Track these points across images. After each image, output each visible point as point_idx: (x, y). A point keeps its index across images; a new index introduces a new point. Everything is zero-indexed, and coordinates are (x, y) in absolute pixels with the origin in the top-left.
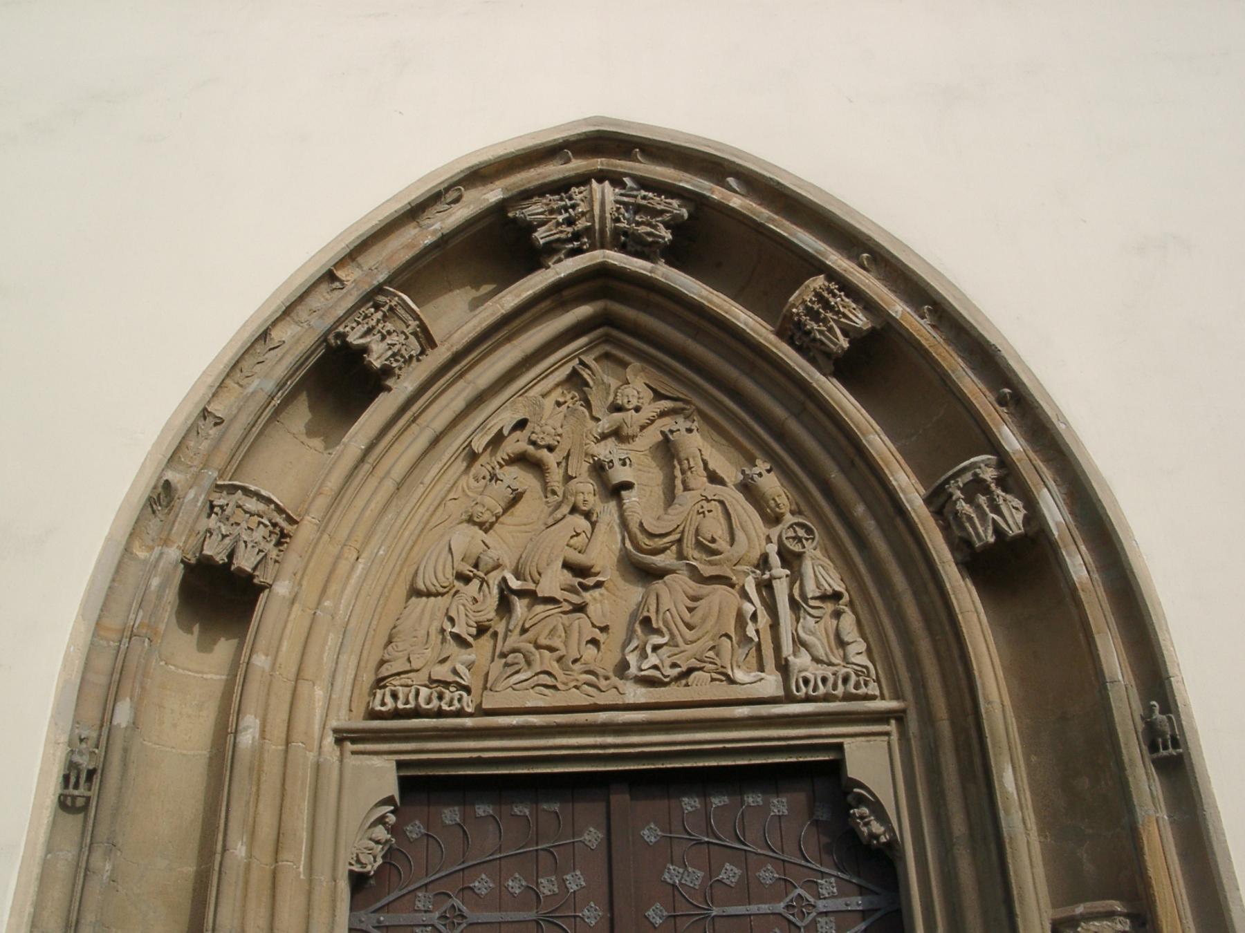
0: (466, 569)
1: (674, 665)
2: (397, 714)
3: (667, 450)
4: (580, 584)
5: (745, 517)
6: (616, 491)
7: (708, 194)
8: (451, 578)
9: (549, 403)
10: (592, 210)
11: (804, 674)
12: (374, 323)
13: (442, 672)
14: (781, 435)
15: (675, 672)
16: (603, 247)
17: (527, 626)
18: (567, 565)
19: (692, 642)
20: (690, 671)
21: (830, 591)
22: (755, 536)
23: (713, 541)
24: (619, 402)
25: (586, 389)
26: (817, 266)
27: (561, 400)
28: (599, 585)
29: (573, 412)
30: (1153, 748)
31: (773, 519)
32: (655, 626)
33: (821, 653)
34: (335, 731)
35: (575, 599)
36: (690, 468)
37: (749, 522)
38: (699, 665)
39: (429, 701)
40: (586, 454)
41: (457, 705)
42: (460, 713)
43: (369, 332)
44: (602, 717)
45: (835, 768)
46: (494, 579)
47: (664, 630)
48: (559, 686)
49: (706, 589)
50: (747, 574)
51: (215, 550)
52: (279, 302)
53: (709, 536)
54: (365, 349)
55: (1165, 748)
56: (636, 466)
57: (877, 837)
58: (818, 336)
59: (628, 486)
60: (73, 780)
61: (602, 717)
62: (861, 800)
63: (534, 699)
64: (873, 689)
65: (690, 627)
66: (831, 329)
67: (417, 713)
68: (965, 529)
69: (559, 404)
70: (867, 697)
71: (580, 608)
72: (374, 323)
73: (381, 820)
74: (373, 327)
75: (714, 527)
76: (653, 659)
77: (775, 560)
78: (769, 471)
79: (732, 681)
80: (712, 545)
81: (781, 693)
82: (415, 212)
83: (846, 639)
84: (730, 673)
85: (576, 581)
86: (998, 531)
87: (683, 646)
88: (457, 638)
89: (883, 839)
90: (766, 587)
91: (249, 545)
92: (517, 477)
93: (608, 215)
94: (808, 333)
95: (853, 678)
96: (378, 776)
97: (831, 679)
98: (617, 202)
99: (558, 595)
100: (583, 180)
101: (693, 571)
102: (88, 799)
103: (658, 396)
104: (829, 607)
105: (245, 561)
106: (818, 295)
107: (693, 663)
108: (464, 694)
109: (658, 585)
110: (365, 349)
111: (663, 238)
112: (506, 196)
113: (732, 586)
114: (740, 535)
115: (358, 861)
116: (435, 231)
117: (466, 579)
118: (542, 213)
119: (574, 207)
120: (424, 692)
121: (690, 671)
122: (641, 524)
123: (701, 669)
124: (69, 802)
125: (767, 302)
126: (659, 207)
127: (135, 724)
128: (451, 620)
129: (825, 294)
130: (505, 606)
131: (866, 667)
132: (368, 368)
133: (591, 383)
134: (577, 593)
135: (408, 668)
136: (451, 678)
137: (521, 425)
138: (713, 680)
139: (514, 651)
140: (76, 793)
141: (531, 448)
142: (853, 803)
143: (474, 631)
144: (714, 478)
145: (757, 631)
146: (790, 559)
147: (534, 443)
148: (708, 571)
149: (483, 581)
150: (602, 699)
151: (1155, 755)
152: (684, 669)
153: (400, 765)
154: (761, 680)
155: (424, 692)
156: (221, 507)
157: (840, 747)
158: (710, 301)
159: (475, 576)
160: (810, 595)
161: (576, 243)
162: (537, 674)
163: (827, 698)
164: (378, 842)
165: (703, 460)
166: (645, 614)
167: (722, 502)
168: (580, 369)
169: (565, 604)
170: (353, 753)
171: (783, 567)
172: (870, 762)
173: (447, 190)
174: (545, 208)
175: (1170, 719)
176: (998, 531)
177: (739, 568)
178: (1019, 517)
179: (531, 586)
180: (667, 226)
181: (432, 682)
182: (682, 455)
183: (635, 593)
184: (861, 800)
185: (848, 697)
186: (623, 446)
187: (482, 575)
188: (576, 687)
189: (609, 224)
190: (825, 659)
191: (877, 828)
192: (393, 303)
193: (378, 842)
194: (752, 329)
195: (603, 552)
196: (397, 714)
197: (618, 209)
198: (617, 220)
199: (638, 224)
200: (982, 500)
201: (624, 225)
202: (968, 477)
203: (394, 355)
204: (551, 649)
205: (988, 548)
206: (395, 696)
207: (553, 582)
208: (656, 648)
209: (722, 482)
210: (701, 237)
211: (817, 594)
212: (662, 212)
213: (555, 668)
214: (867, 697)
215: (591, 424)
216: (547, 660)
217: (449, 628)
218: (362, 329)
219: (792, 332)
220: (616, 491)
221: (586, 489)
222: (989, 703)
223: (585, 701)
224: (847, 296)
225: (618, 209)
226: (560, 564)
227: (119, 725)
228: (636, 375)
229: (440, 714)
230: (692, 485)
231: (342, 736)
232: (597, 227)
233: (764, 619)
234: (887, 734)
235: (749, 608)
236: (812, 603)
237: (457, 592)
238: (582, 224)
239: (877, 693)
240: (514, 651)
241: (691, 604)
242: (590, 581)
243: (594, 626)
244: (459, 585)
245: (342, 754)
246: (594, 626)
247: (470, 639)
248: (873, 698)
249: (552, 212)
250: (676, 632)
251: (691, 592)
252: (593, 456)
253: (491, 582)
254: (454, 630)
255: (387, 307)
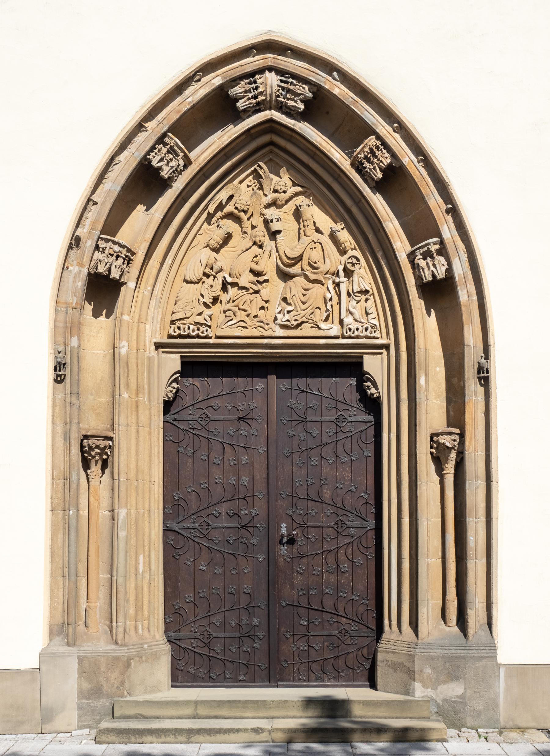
0: (207, 270)
1: (296, 320)
2: (180, 336)
3: (298, 214)
4: (257, 281)
5: (330, 252)
6: (274, 235)
7: (323, 85)
8: (201, 275)
9: (244, 184)
10: (266, 90)
11: (349, 326)
12: (163, 155)
13: (200, 319)
14: (349, 211)
15: (295, 323)
16: (270, 109)
17: (234, 299)
18: (251, 271)
19: (304, 310)
20: (303, 323)
21: (364, 289)
22: (334, 261)
23: (315, 263)
24: (276, 188)
25: (260, 179)
26: (371, 131)
27: (249, 184)
28: (266, 281)
29: (255, 193)
30: (479, 372)
31: (343, 252)
32: (289, 301)
33: (357, 317)
34: (155, 343)
35: (256, 288)
36: (308, 226)
37: (332, 254)
38: (307, 320)
39: (193, 331)
40: (261, 214)
41: (205, 334)
42: (207, 337)
43: (161, 160)
44: (266, 341)
45: (359, 364)
46: (220, 276)
47: (292, 303)
48: (248, 327)
49: (310, 285)
50: (329, 279)
51: (102, 269)
52: (118, 142)
53: (314, 260)
54: (160, 168)
55: (483, 373)
56: (282, 218)
57: (373, 394)
58: (369, 171)
59: (279, 232)
60: (58, 368)
61: (266, 341)
62: (368, 380)
63: (238, 332)
64: (377, 334)
65: (304, 303)
66: (374, 168)
67: (188, 336)
68: (420, 272)
69: (248, 186)
70: (374, 338)
71: (257, 292)
72: (163, 155)
73: (176, 380)
74: (163, 157)
75: (316, 255)
76: (287, 317)
77: (342, 273)
78: (342, 229)
79: (319, 328)
80: (315, 265)
81: (339, 334)
82: (179, 89)
83: (369, 312)
84: (319, 324)
85: (255, 279)
86: (433, 275)
87: (300, 312)
88: (205, 304)
89: (375, 396)
90: (337, 285)
91: (118, 267)
92: (229, 225)
93: (274, 94)
94: (365, 168)
95: (370, 329)
96: (173, 362)
97: (360, 328)
98: (278, 86)
99: (248, 285)
100: (261, 71)
101: (306, 277)
102: (65, 375)
103: (294, 184)
104: (363, 297)
105: (115, 274)
106: (371, 150)
107: (304, 319)
108: (208, 328)
109: (290, 283)
110: (160, 168)
111: (300, 109)
112: (224, 81)
113: (323, 285)
114: (327, 260)
115: (167, 396)
116: (189, 103)
117: (208, 276)
118: (241, 93)
119: (257, 88)
120: (192, 327)
121: (303, 323)
122: (285, 252)
123: (307, 322)
124: (59, 379)
125: (348, 145)
126: (299, 92)
127: (79, 345)
128: (202, 295)
129: (375, 149)
130: (224, 288)
131: (375, 325)
132: (162, 178)
133: (263, 177)
134: (256, 285)
135: (184, 316)
136: (203, 321)
137: (231, 197)
138: (312, 327)
139: (229, 310)
140: (60, 373)
141: (236, 211)
142: (366, 380)
143: (212, 301)
144: (318, 230)
145: (332, 306)
146: (348, 273)
147: (236, 208)
148: (312, 277)
149: (215, 277)
150: (266, 334)
151: (479, 375)
152: (300, 322)
153: (181, 356)
154: (331, 328)
155: (192, 327)
156: (103, 249)
157: (362, 357)
158: (320, 145)
159: (212, 275)
160: (355, 291)
161: (258, 108)
162: (239, 322)
163: (358, 337)
164: (174, 388)
165: (314, 222)
166: (285, 296)
167: (321, 244)
168: (258, 168)
169: (251, 289)
170: (163, 352)
171: (345, 277)
172: (373, 364)
173: (195, 75)
174: (243, 90)
175: (487, 362)
176: (433, 275)
177: (326, 276)
178: (444, 269)
179: (236, 280)
180: (302, 101)
181: (196, 323)
182: (304, 218)
183: (281, 284)
184: (368, 380)
185: (367, 337)
186: (278, 210)
187: (215, 274)
188: (255, 328)
189: (274, 98)
190: (359, 320)
191: (373, 390)
192: (172, 144)
193: (174, 388)
194: (339, 162)
195: (268, 265)
196: (180, 336)
197: (279, 90)
198: (278, 96)
199: (288, 99)
200: (429, 260)
201: (281, 99)
202: (426, 249)
203: (173, 171)
204: (245, 310)
205: (428, 283)
206: (179, 328)
207: (246, 279)
208: (289, 312)
209: (321, 233)
210: (319, 106)
211: (359, 290)
212: (301, 94)
213: (246, 319)
214: (374, 338)
215: (264, 198)
216: (242, 315)
217: (201, 298)
218: (158, 158)
219: (359, 167)
220: (274, 235)
221: (261, 232)
222: (419, 348)
223: (259, 334)
224: (384, 149)
225: (279, 90)
226: (249, 271)
227: (74, 346)
228: (285, 174)
229: (198, 336)
230: (307, 234)
231: (158, 346)
232: (268, 99)
233: (335, 299)
234: (381, 353)
235: (328, 296)
236: (356, 294)
237: (203, 282)
238: (261, 98)
239: (379, 336)
240: (229, 310)
241: (304, 292)
242: (261, 279)
243: (263, 300)
244: (204, 278)
245: (158, 353)
246: (263, 300)
247: (210, 305)
248: (378, 338)
249: (246, 92)
250: (297, 305)
251: (305, 287)
252: (264, 215)
253: (218, 278)
254: (204, 300)
255: (169, 146)
